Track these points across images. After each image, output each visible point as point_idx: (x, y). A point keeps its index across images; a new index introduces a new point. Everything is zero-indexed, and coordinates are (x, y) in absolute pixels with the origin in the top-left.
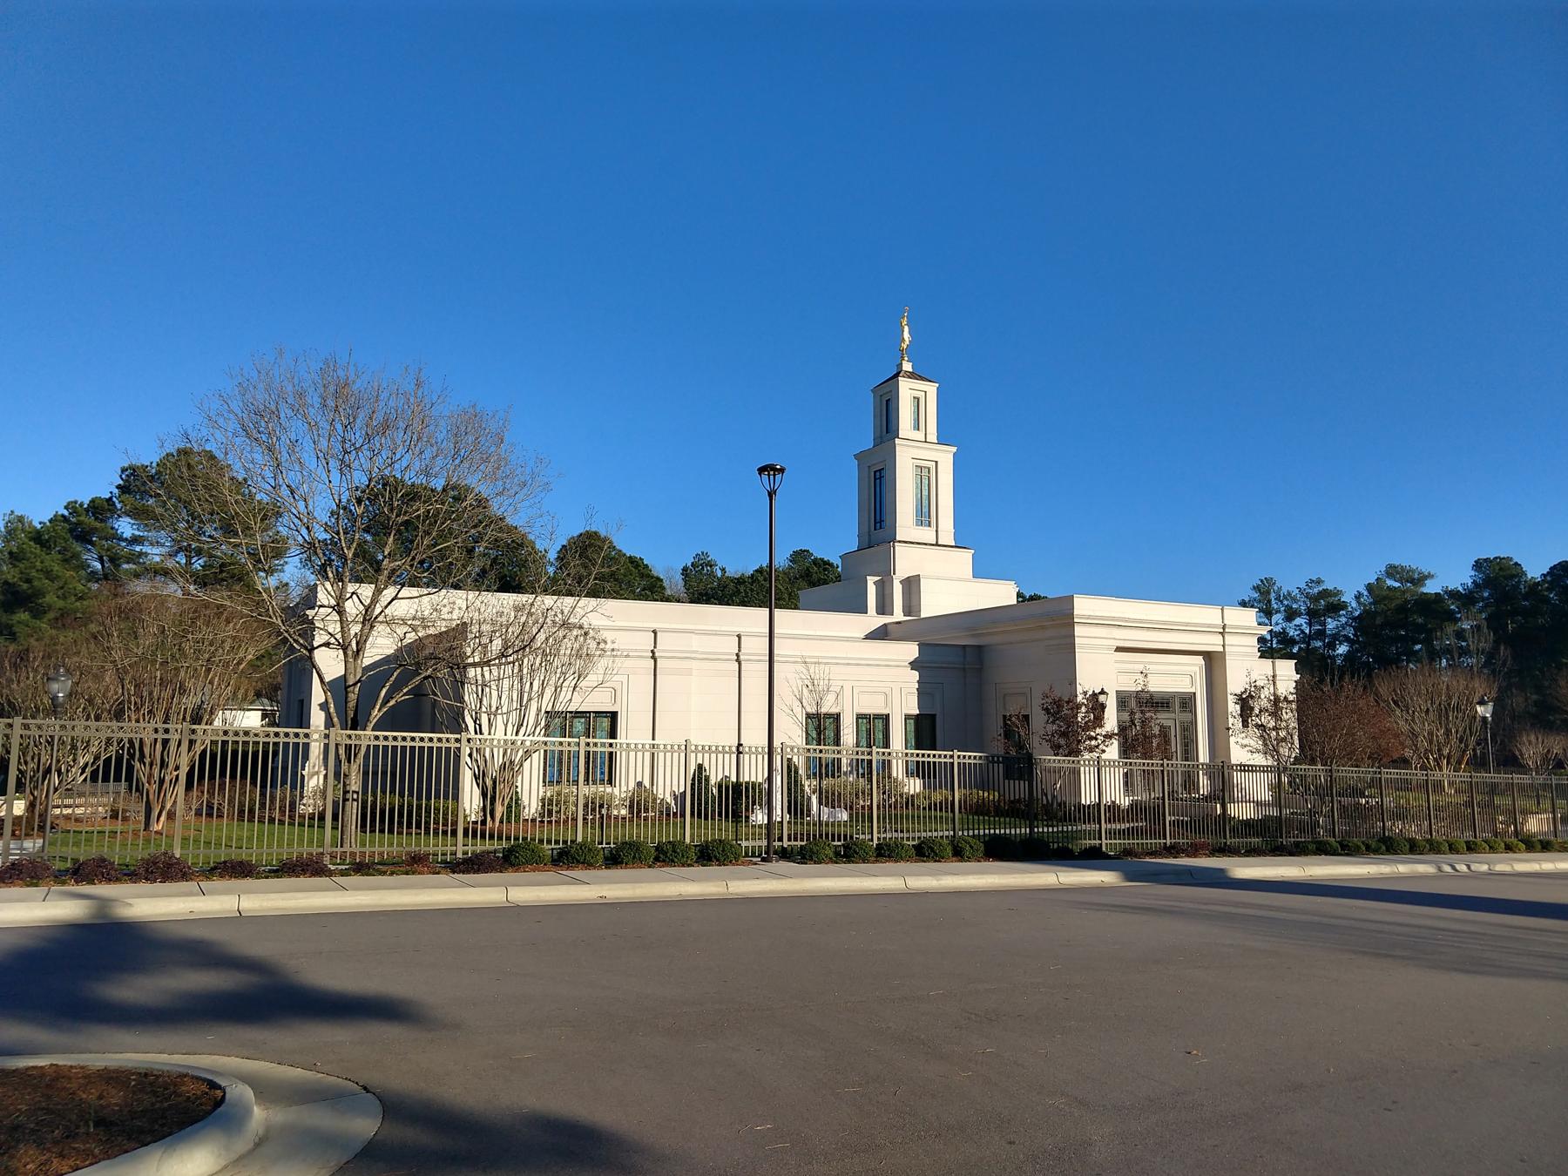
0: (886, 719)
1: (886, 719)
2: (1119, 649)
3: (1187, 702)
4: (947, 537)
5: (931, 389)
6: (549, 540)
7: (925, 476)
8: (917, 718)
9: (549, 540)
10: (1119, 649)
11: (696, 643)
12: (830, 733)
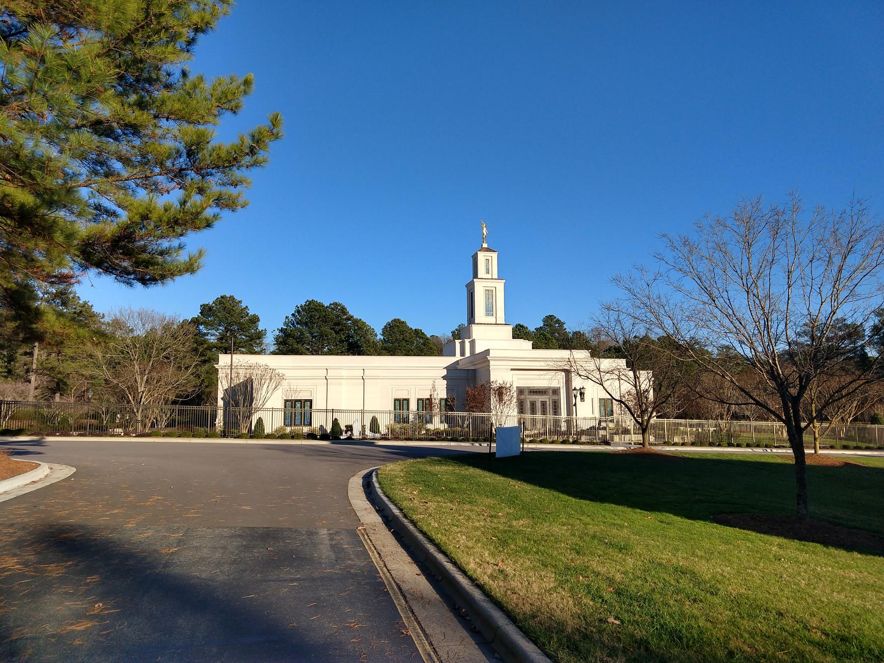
0: (408, 400)
1: (408, 400)
2: (512, 370)
3: (556, 391)
4: (501, 319)
5: (494, 255)
6: (377, 325)
7: (490, 294)
8: (446, 400)
9: (377, 325)
10: (512, 370)
11: (344, 373)
12: (405, 407)
